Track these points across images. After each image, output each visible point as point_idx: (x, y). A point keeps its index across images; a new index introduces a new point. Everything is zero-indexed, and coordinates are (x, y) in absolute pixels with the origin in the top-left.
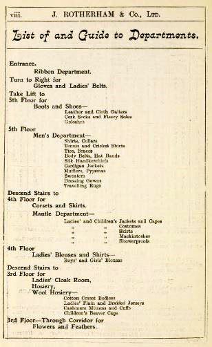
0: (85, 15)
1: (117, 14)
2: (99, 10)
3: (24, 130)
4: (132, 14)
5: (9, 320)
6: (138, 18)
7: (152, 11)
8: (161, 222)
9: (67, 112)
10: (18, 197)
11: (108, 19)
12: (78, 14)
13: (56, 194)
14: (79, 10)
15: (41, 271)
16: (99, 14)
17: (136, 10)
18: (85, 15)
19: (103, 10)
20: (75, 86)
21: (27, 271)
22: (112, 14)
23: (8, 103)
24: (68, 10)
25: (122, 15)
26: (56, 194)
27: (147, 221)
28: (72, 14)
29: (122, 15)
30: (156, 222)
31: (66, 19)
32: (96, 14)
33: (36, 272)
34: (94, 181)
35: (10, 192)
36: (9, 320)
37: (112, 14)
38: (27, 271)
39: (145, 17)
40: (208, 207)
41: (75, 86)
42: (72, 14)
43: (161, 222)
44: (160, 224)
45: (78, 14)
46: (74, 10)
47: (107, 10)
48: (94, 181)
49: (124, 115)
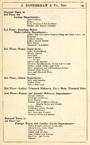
0: (35, 6)
1: (49, 5)
3: (11, 30)
4: (55, 5)
5: (5, 49)
6: (57, 7)
7: (63, 4)
8: (46, 51)
9: (28, 41)
10: (9, 120)
11: (45, 7)
12: (32, 6)
13: (25, 119)
15: (18, 14)
16: (41, 5)
17: (57, 4)
18: (35, 6)
19: (43, 4)
21: (12, 14)
22: (46, 5)
23: (3, 16)
24: (28, 4)
25: (51, 6)
26: (25, 119)
28: (29, 6)
29: (51, 6)
31: (27, 7)
32: (40, 5)
33: (16, 120)
35: (6, 118)
36: (5, 49)
38: (12, 14)
39: (60, 7)
40: (87, 117)
42: (29, 6)
43: (46, 51)
46: (30, 4)
47: (44, 4)
49: (51, 72)
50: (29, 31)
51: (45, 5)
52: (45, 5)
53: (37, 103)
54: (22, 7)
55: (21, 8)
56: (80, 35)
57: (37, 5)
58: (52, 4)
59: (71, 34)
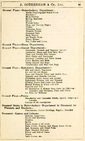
0: (33, 5)
1: (46, 5)
2: (39, 3)
4: (52, 5)
7: (60, 3)
8: (61, 58)
12: (31, 5)
14: (31, 3)
18: (33, 5)
19: (41, 3)
20: (43, 98)
22: (44, 5)
24: (5, 9)
25: (48, 5)
27: (41, 98)
28: (28, 5)
29: (48, 5)
30: (59, 111)
34: (8, 106)
37: (44, 5)
41: (43, 98)
42: (28, 5)
43: (61, 58)
44: (61, 83)
45: (31, 5)
48: (8, 106)
50: (33, 18)
51: (43, 5)
52: (43, 5)
53: (46, 60)
54: (21, 6)
55: (20, 7)
56: (63, 110)
57: (36, 4)
58: (50, 4)
59: (57, 73)
